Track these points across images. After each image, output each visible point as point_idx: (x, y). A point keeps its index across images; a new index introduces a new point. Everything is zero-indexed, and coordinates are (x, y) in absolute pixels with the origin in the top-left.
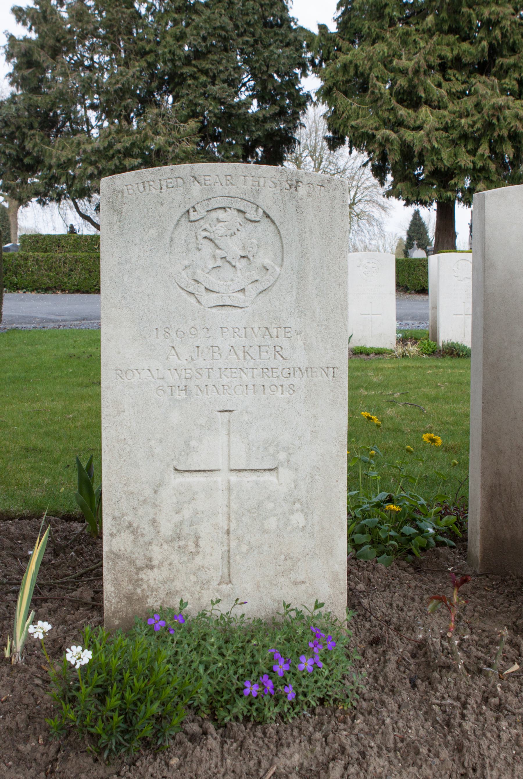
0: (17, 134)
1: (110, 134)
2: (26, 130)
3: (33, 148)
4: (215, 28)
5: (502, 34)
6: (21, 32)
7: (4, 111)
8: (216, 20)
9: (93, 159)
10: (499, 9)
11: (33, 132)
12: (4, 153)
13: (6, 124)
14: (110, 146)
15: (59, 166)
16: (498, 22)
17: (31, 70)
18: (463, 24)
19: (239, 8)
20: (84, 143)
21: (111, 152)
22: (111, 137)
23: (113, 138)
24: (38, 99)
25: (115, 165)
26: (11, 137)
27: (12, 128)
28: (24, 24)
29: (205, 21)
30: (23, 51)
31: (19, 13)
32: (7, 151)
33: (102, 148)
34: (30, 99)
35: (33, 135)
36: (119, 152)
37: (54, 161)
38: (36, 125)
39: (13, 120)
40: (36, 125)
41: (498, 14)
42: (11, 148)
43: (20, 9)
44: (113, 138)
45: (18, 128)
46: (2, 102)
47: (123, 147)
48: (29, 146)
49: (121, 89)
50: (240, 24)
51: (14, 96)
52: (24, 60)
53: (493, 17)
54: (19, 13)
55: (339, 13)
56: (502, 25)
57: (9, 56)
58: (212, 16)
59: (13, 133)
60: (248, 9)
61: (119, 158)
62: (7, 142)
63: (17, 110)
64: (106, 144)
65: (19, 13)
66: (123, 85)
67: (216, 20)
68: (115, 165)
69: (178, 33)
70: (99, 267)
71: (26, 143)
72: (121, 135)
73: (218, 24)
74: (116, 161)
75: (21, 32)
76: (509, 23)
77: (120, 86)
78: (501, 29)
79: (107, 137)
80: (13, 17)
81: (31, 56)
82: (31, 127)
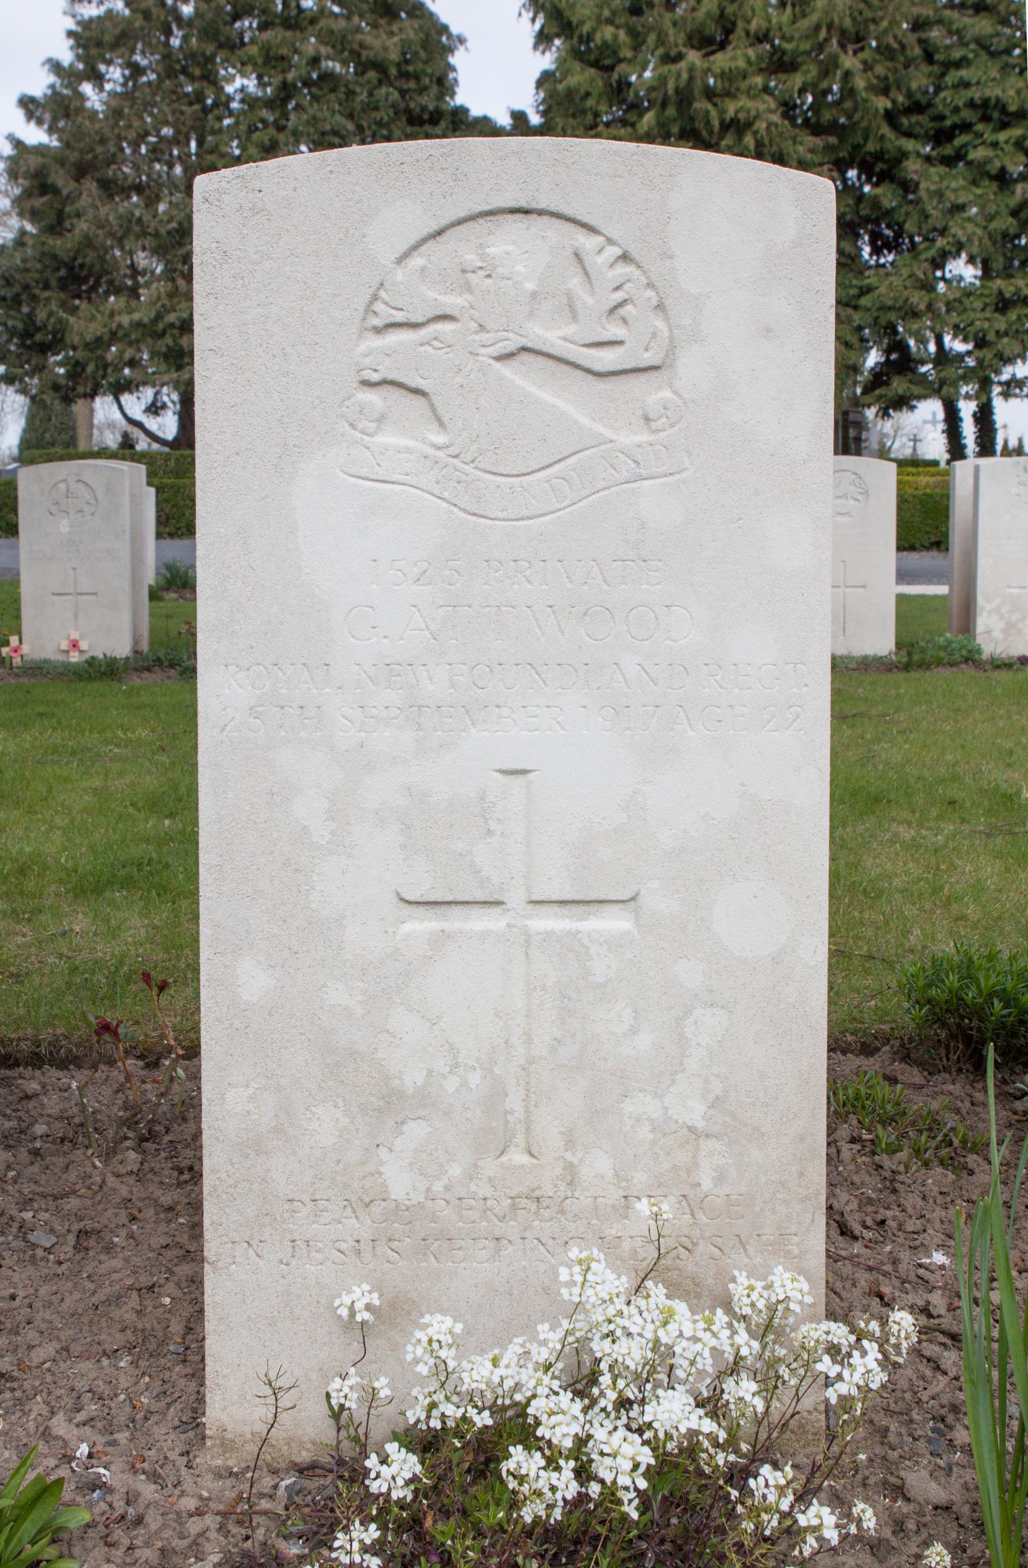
0: (24, 297)
1: (159, 298)
2: (36, 291)
3: (48, 318)
4: (323, 134)
5: (757, 141)
6: (35, 135)
7: (5, 262)
8: (325, 120)
9: (133, 337)
10: (750, 104)
11: (47, 294)
12: (5, 324)
13: (8, 282)
14: (159, 317)
15: (87, 346)
16: (749, 125)
17: (45, 199)
18: (699, 125)
19: (362, 101)
20: (120, 313)
21: (161, 326)
22: (159, 304)
23: (163, 306)
24: (56, 243)
25: (167, 346)
26: (17, 301)
27: (17, 289)
28: (40, 122)
29: (308, 123)
30: (32, 170)
31: (28, 105)
32: (10, 323)
33: (146, 320)
34: (44, 243)
35: (47, 299)
36: (172, 325)
37: (76, 340)
38: (54, 283)
39: (18, 276)
40: (54, 283)
41: (749, 111)
42: (15, 318)
43: (32, 100)
44: (163, 306)
45: (26, 287)
46: (3, 246)
47: (178, 318)
48: (41, 315)
49: (177, 231)
50: (365, 124)
51: (23, 233)
52: (36, 183)
53: (742, 116)
54: (28, 105)
55: (542, 95)
56: (755, 128)
57: (13, 174)
58: (319, 115)
59: (18, 295)
60: (378, 101)
61: (173, 336)
62: (10, 308)
63: (24, 261)
64: (153, 315)
65: (31, 106)
66: (180, 224)
67: (325, 120)
68: (167, 346)
69: (267, 142)
70: (832, 696)
71: (38, 311)
72: (176, 300)
73: (328, 127)
74: (169, 340)
75: (35, 135)
76: (764, 125)
77: (174, 225)
78: (755, 133)
79: (155, 303)
80: (20, 114)
81: (45, 176)
82: (46, 286)
